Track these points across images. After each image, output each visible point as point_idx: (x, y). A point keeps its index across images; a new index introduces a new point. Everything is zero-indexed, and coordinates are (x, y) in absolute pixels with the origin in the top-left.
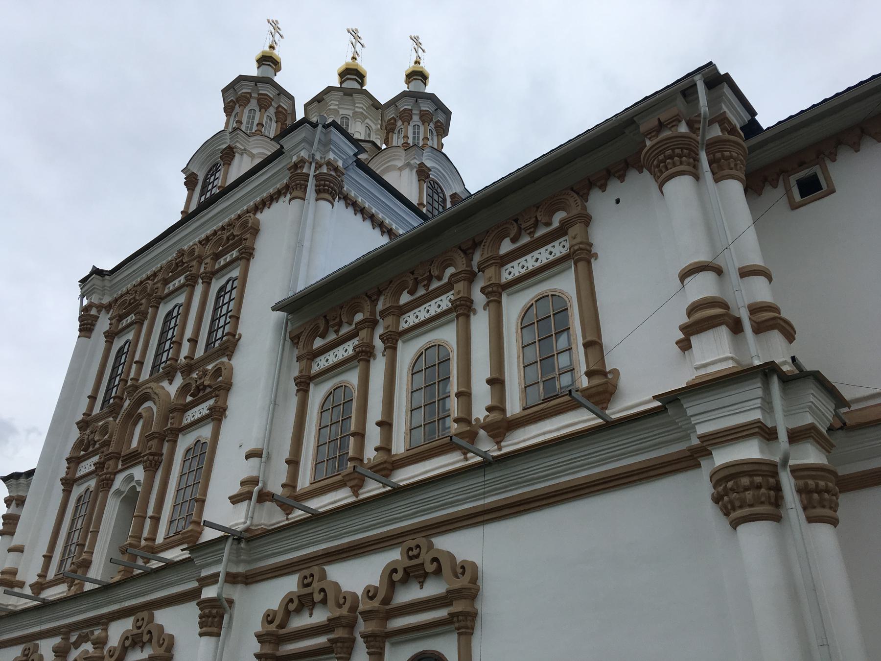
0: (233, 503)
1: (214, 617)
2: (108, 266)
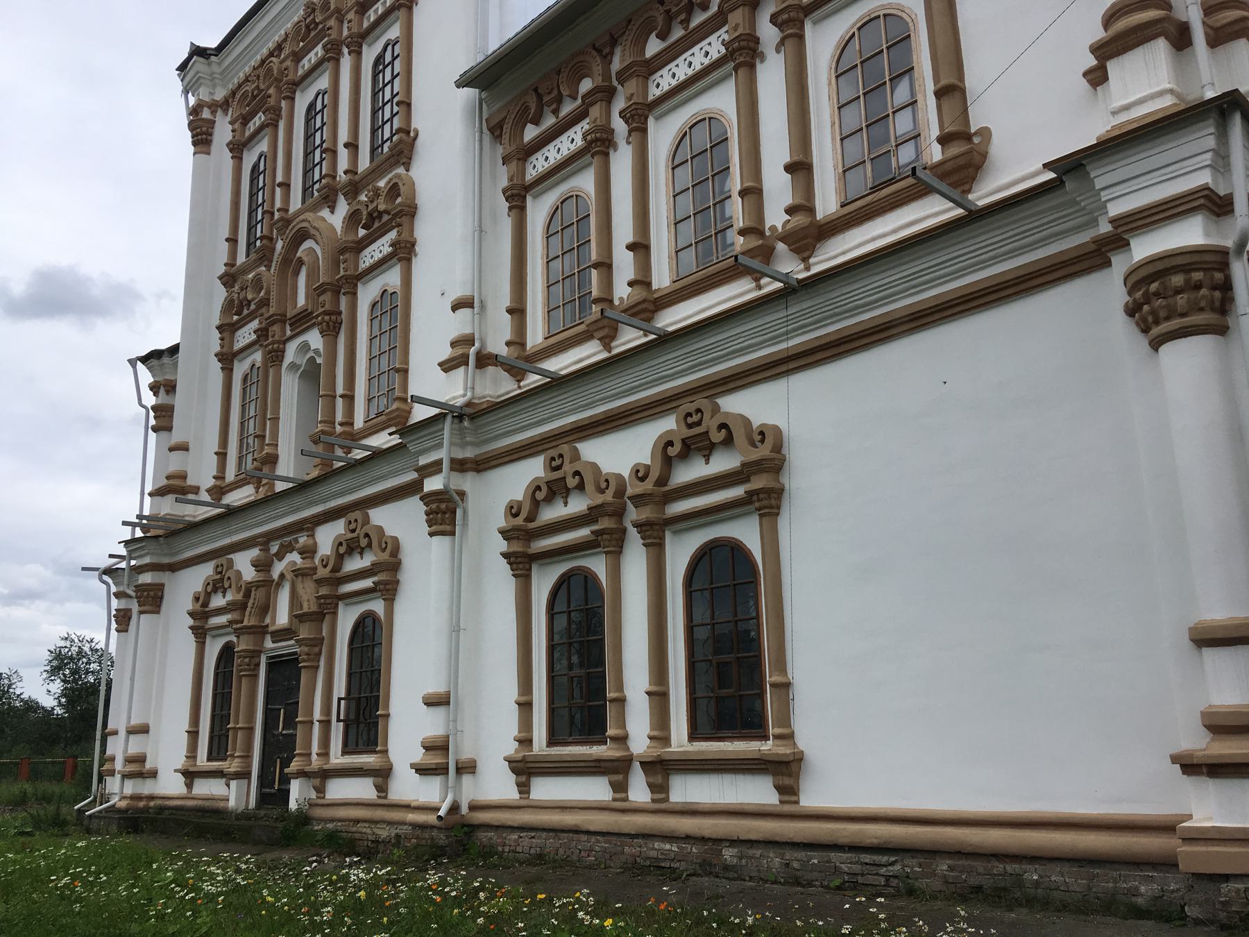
0: (446, 371)
1: (444, 513)
2: (212, 42)
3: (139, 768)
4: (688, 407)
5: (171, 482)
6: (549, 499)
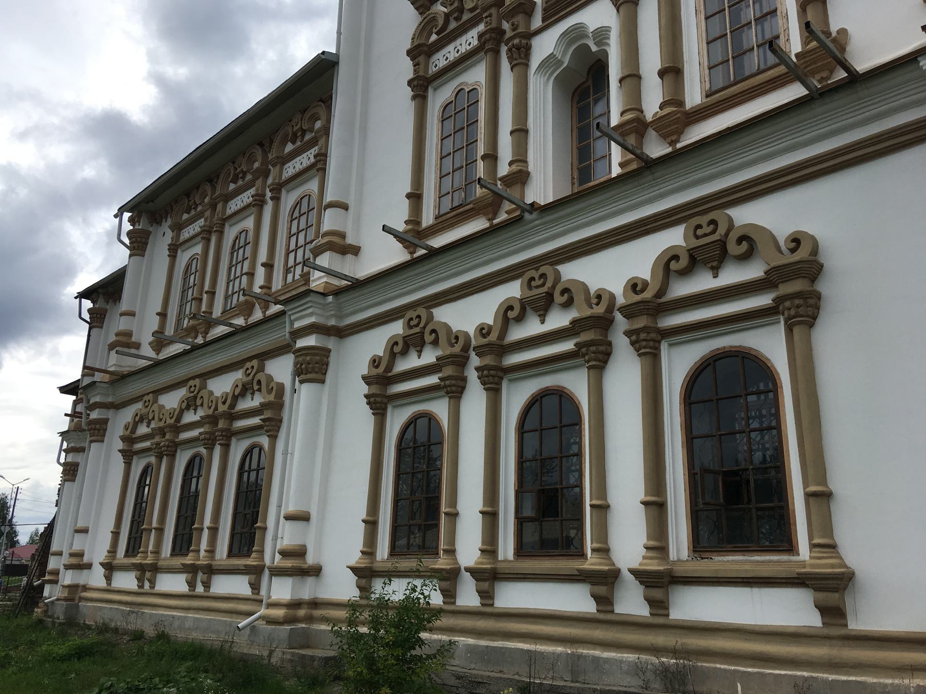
3: (298, 564)
4: (411, 314)
5: (119, 338)
6: (404, 353)
